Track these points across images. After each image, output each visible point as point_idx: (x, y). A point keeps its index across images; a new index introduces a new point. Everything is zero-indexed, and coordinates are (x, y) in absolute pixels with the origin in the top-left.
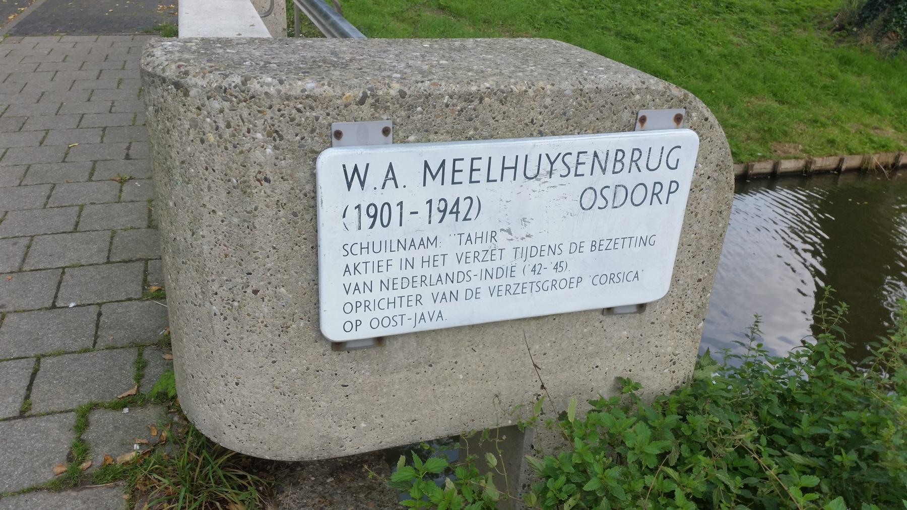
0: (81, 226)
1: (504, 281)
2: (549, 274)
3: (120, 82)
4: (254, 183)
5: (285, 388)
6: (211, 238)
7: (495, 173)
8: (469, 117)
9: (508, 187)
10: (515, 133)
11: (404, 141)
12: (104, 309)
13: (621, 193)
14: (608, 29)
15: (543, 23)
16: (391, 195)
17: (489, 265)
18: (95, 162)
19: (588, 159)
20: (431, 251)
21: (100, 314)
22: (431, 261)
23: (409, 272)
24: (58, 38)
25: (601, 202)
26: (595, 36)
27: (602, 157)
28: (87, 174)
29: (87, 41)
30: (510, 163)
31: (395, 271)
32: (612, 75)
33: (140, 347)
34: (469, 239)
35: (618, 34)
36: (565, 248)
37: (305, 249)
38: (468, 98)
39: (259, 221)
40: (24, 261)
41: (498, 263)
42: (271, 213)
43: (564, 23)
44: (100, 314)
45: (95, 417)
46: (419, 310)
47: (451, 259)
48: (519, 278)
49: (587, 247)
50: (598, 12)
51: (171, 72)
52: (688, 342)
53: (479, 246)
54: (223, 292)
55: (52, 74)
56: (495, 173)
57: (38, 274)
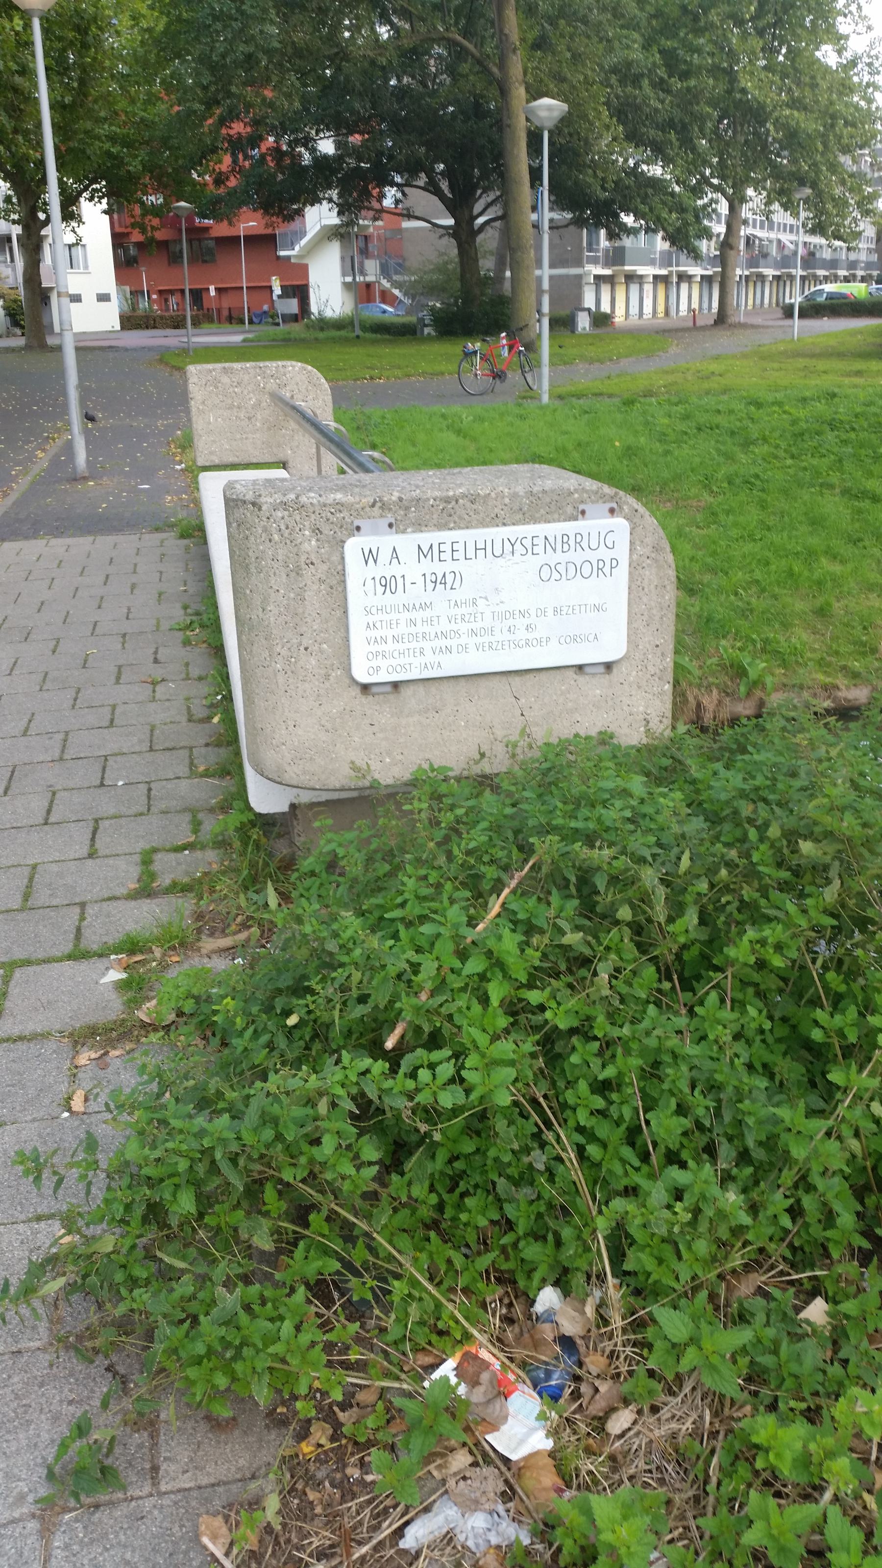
0: (116, 722)
1: (487, 639)
2: (522, 635)
3: (133, 587)
4: (304, 567)
5: (329, 726)
6: (276, 611)
7: (471, 553)
8: (449, 514)
9: (481, 564)
10: (483, 524)
11: (404, 532)
12: (153, 785)
13: (572, 568)
14: (831, 487)
15: (725, 485)
16: (396, 570)
17: (473, 626)
18: (120, 667)
19: (540, 541)
20: (427, 613)
21: (150, 790)
22: (430, 621)
23: (413, 630)
24: (44, 542)
25: (556, 575)
26: (806, 497)
27: (551, 540)
28: (113, 679)
29: (82, 544)
30: (480, 545)
31: (403, 629)
32: (555, 479)
33: (193, 811)
34: (456, 604)
35: (846, 492)
36: (533, 612)
37: (339, 613)
38: (447, 500)
39: (307, 594)
40: (63, 752)
41: (480, 624)
42: (315, 587)
43: (758, 483)
44: (150, 790)
45: (158, 857)
46: (423, 660)
47: (444, 620)
48: (498, 637)
49: (550, 612)
50: (815, 462)
51: (250, 497)
52: (658, 702)
53: (464, 610)
54: (284, 652)
55: (48, 582)
56: (471, 553)
57: (80, 762)
